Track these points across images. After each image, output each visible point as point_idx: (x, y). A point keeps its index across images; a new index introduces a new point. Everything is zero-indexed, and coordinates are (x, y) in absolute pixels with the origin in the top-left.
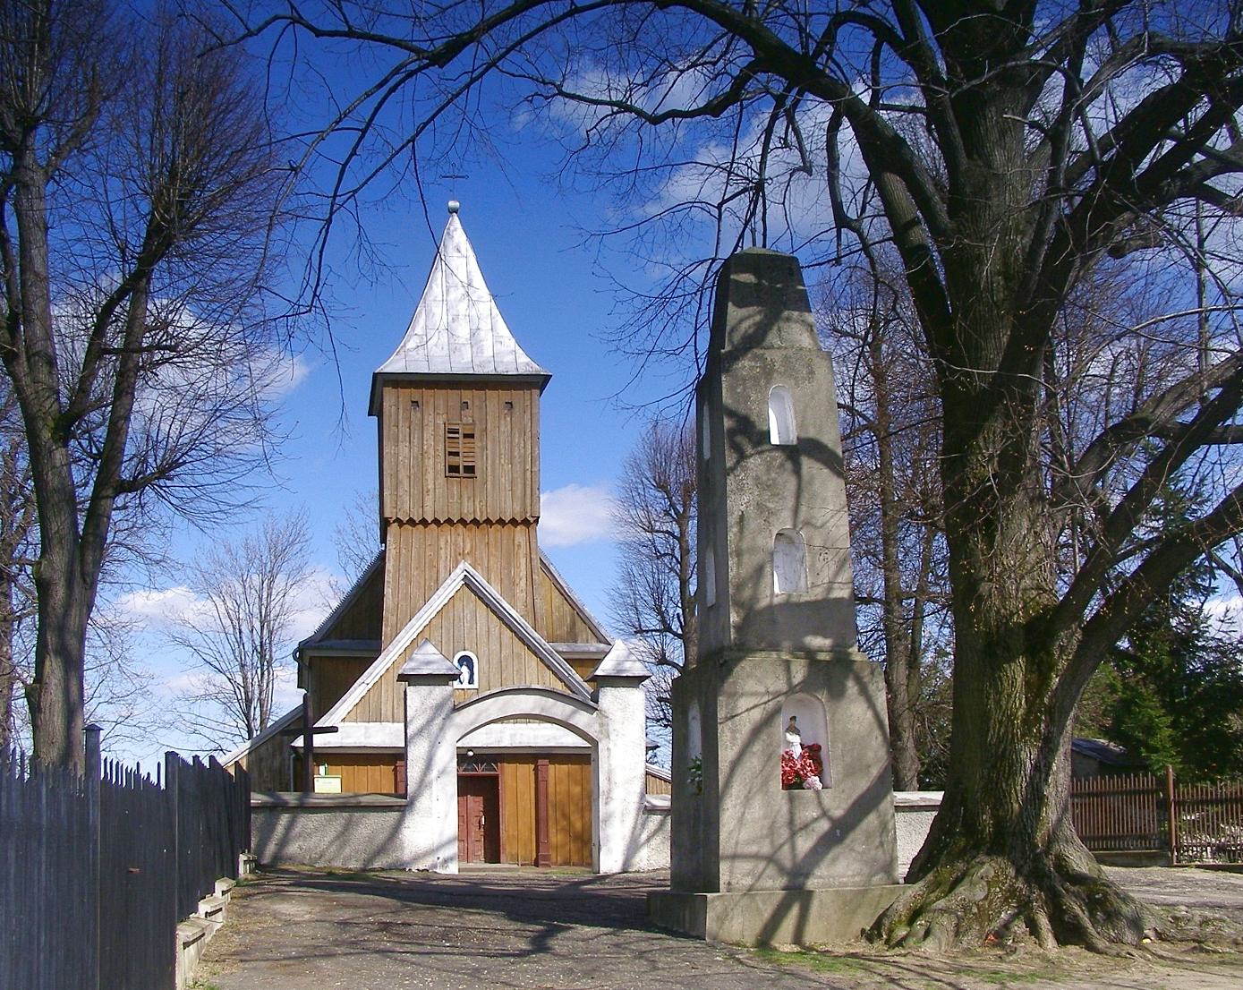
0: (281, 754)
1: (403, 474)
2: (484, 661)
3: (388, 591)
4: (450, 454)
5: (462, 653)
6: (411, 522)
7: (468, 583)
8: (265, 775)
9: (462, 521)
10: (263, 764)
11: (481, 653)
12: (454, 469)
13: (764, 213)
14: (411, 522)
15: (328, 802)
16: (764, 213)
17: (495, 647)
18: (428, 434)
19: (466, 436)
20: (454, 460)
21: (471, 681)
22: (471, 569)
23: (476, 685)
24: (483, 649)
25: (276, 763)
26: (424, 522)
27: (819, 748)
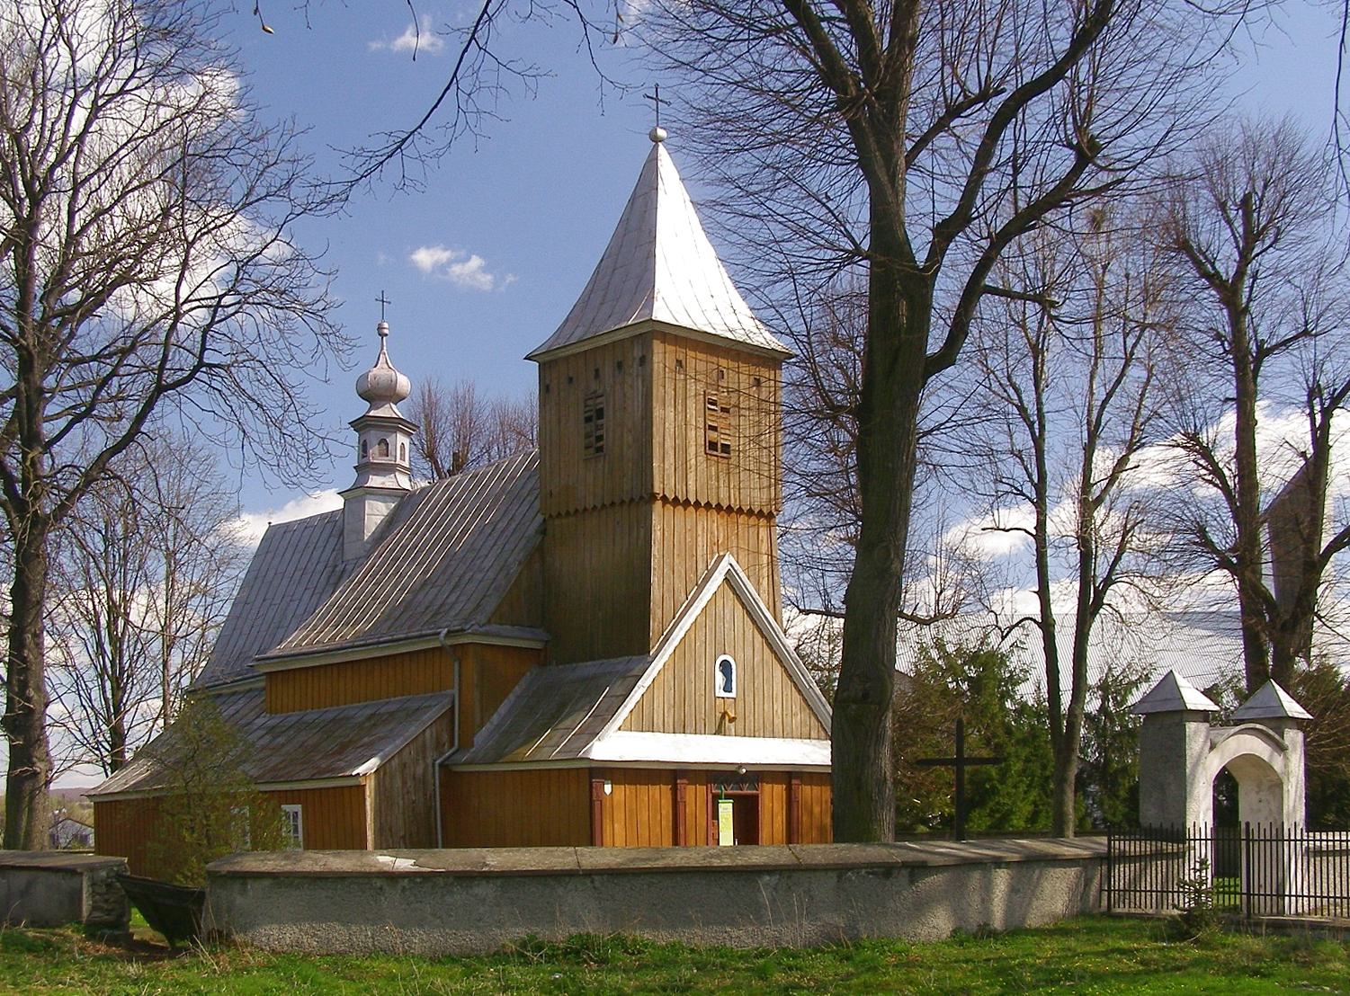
0: (424, 758)
1: (669, 443)
2: (741, 666)
3: (654, 579)
4: (712, 428)
5: (722, 658)
6: (676, 501)
7: (729, 580)
8: (409, 784)
9: (719, 507)
10: (407, 771)
11: (738, 658)
12: (713, 445)
13: (207, 299)
14: (676, 501)
15: (1270, 742)
16: (207, 299)
17: (749, 652)
18: (691, 404)
19: (723, 410)
20: (713, 435)
21: (727, 688)
22: (734, 563)
23: (733, 695)
24: (740, 655)
25: (420, 770)
26: (687, 503)
27: (591, 843)
